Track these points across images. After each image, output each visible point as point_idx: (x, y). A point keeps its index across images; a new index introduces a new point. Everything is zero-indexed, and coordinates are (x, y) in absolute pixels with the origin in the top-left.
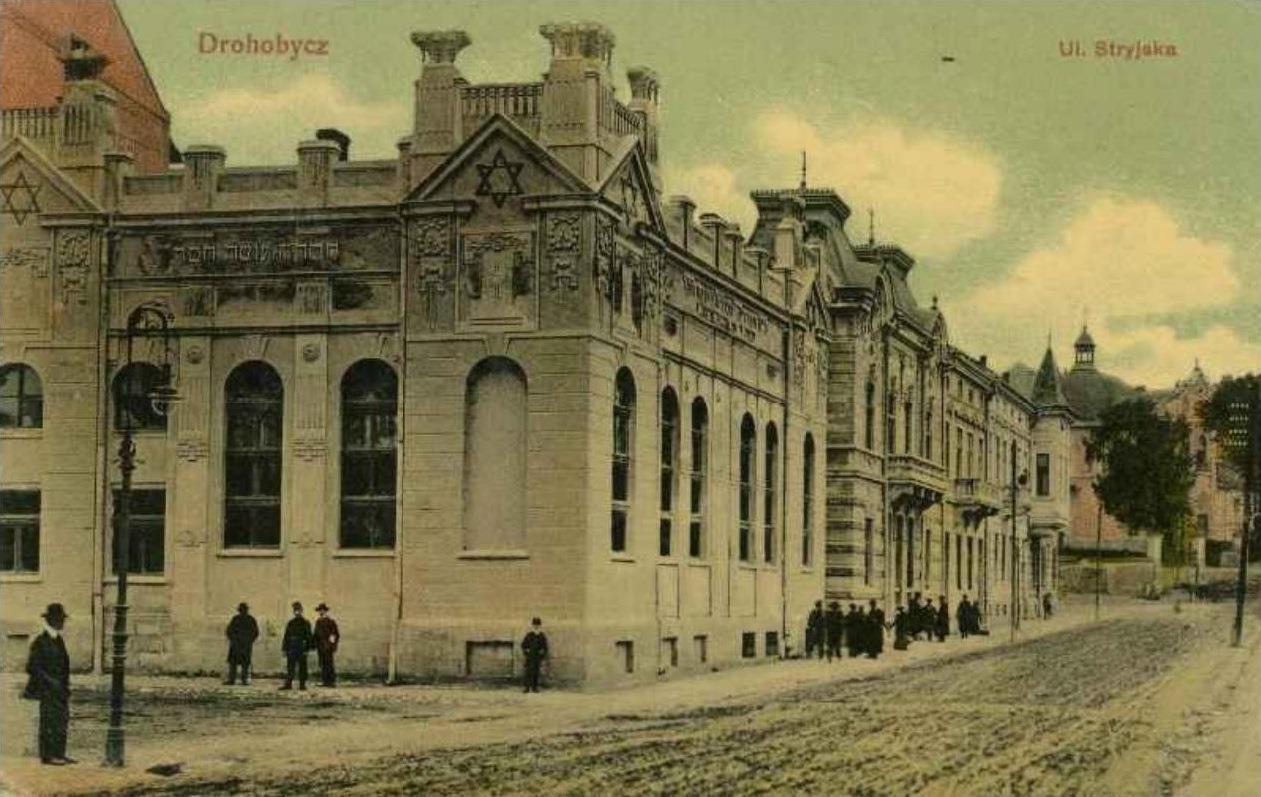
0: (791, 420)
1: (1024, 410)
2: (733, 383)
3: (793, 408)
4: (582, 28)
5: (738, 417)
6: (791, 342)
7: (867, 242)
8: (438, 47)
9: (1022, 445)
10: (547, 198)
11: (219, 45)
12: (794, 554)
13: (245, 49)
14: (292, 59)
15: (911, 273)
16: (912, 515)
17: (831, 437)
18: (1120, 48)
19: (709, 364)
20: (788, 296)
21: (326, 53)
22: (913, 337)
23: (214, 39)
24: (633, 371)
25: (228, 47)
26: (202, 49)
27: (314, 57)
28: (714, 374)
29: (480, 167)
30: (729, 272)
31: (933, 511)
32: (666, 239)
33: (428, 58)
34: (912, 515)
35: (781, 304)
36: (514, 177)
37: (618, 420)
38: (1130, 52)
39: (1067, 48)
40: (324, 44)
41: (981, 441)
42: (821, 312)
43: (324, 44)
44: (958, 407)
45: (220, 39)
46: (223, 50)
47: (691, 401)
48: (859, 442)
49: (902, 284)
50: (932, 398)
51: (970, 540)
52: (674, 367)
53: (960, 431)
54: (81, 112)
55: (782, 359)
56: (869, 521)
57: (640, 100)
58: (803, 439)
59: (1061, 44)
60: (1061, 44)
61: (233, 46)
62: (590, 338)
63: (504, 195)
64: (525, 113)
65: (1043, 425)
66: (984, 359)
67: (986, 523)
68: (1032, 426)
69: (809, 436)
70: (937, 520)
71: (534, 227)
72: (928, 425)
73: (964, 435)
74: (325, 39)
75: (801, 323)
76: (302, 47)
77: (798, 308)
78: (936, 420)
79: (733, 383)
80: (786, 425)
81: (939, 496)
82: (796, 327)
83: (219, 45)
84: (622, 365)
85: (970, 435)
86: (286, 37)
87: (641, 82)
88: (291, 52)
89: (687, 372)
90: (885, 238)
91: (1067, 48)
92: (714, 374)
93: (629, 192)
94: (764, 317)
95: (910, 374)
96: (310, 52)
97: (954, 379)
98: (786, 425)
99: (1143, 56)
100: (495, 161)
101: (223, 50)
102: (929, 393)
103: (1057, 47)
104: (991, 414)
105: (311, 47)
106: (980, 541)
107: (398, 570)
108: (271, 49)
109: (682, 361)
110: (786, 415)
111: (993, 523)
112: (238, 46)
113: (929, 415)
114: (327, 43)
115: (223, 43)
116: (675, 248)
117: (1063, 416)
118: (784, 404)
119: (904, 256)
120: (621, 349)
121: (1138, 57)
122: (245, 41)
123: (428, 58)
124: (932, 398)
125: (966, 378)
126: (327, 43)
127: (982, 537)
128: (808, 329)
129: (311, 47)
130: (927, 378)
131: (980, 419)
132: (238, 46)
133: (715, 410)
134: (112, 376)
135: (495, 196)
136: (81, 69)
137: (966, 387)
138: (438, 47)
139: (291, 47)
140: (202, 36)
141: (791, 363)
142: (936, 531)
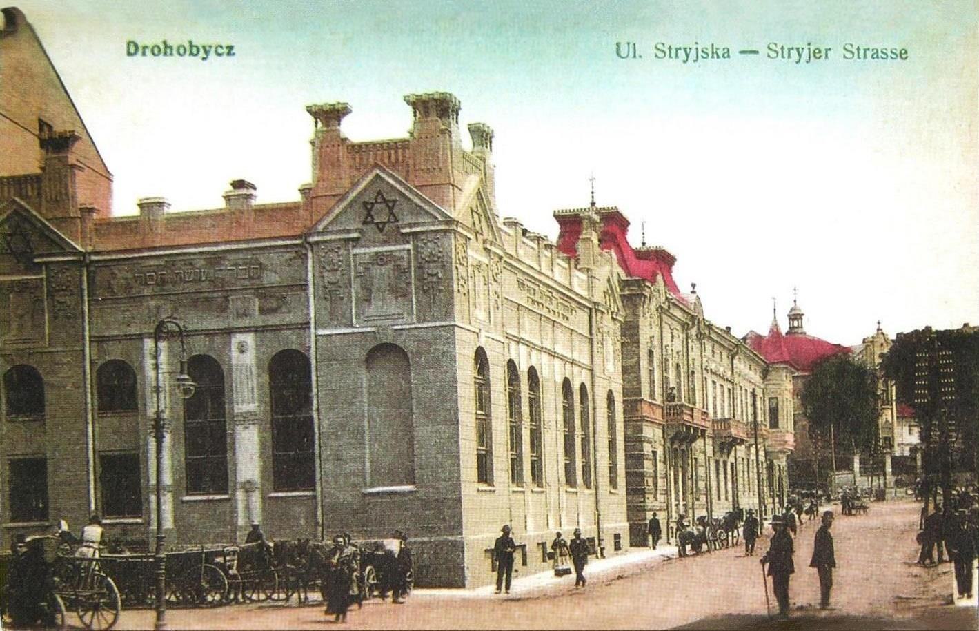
0: (597, 380)
1: (758, 364)
2: (553, 355)
3: (597, 371)
4: (436, 97)
5: (560, 380)
6: (594, 320)
7: (641, 245)
8: (329, 116)
9: (759, 393)
10: (416, 224)
12: (604, 480)
14: (204, 59)
15: (674, 268)
16: (684, 447)
17: (626, 393)
19: (538, 342)
20: (591, 288)
21: (234, 54)
22: (678, 314)
24: (488, 352)
25: (148, 52)
28: (542, 349)
29: (365, 204)
30: (549, 273)
31: (699, 443)
32: (503, 250)
33: (320, 124)
34: (684, 447)
35: (584, 294)
36: (391, 209)
40: (230, 48)
41: (729, 390)
42: (615, 300)
43: (230, 48)
44: (713, 366)
46: (144, 54)
47: (526, 370)
48: (645, 395)
50: (694, 360)
51: (725, 463)
52: (513, 344)
53: (714, 383)
55: (588, 335)
56: (654, 453)
57: (478, 148)
58: (606, 396)
61: (152, 51)
62: (455, 325)
63: (384, 223)
64: (397, 161)
65: (771, 376)
66: (729, 328)
67: (736, 450)
68: (764, 378)
69: (610, 391)
70: (703, 448)
71: (409, 246)
72: (693, 381)
73: (718, 385)
74: (230, 44)
75: (600, 308)
76: (213, 49)
77: (598, 297)
78: (697, 375)
79: (553, 355)
80: (593, 385)
81: (703, 432)
82: (597, 310)
84: (478, 346)
85: (722, 386)
87: (482, 135)
89: (523, 348)
90: (652, 243)
92: (542, 349)
93: (476, 216)
94: (574, 305)
95: (678, 345)
96: (220, 55)
97: (709, 347)
98: (593, 385)
100: (376, 199)
101: (144, 54)
102: (692, 355)
104: (735, 370)
106: (732, 464)
107: (917, 597)
109: (519, 341)
110: (593, 376)
111: (741, 450)
113: (693, 372)
116: (511, 256)
117: (786, 368)
118: (591, 370)
119: (669, 255)
120: (477, 334)
122: (162, 46)
123: (320, 124)
124: (694, 360)
125: (717, 342)
127: (734, 461)
128: (606, 312)
130: (690, 345)
131: (729, 374)
133: (544, 374)
134: (96, 368)
135: (377, 224)
137: (717, 350)
138: (329, 116)
139: (202, 51)
141: (594, 337)
142: (701, 457)
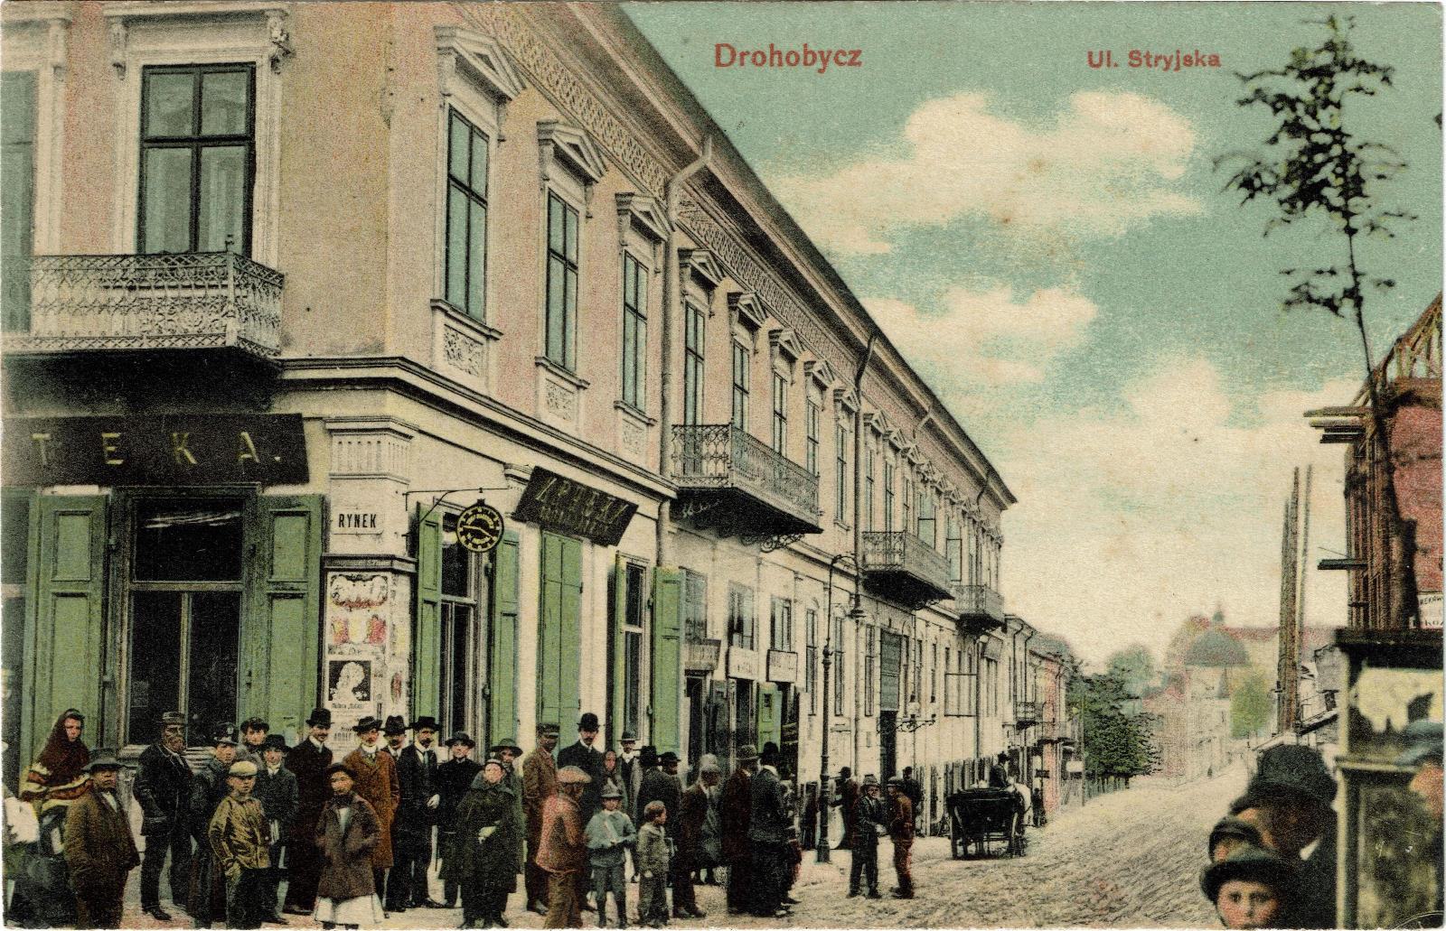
11: (738, 57)
13: (801, 61)
18: (1158, 58)
21: (859, 64)
23: (733, 54)
25: (748, 59)
26: (718, 64)
27: (845, 68)
37: (12, 884)
38: (1168, 63)
39: (1096, 60)
40: (857, 53)
43: (857, 53)
45: (739, 50)
49: (766, 709)
54: (1155, 892)
59: (1090, 54)
60: (1090, 54)
83: (738, 57)
86: (812, 47)
88: (819, 65)
91: (1096, 60)
96: (841, 64)
99: (1184, 68)
101: (742, 64)
103: (1086, 59)
105: (842, 59)
108: (797, 61)
112: (759, 59)
114: (860, 52)
115: (743, 54)
121: (1177, 69)
126: (860, 52)
129: (842, 59)
132: (759, 59)
136: (1258, 163)
139: (819, 57)
140: (718, 47)
